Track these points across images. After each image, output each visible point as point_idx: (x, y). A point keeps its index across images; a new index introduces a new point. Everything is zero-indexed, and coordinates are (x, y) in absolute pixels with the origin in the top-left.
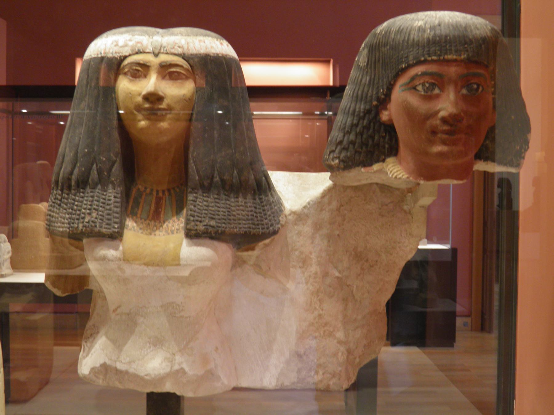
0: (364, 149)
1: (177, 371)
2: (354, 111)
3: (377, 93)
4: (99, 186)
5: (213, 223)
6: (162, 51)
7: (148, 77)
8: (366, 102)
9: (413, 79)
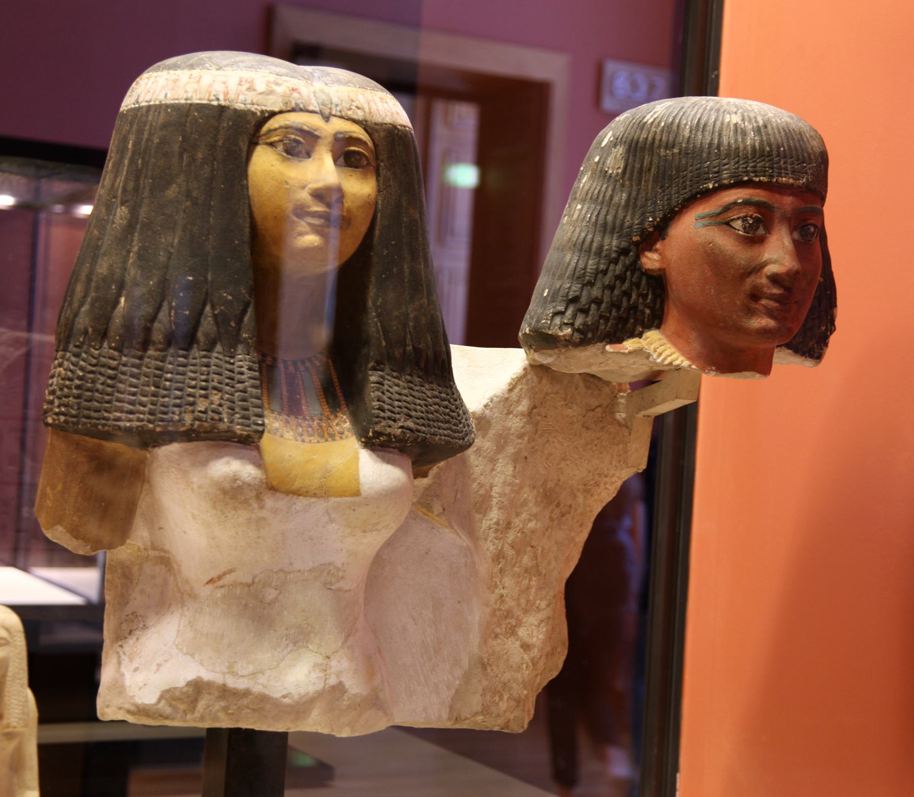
0: (614, 312)
1: (333, 688)
2: (601, 247)
3: (641, 223)
4: (219, 348)
5: (410, 424)
6: (334, 112)
7: (315, 155)
8: (620, 237)
9: (727, 208)
